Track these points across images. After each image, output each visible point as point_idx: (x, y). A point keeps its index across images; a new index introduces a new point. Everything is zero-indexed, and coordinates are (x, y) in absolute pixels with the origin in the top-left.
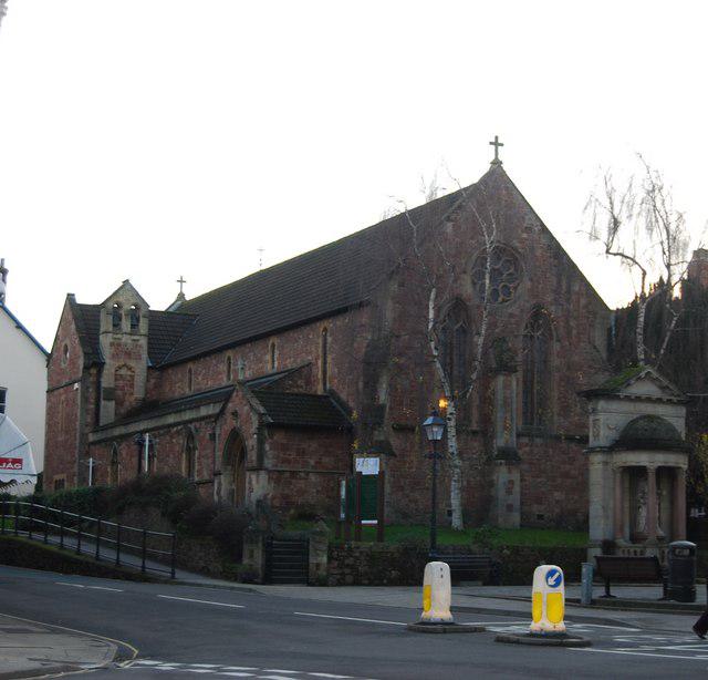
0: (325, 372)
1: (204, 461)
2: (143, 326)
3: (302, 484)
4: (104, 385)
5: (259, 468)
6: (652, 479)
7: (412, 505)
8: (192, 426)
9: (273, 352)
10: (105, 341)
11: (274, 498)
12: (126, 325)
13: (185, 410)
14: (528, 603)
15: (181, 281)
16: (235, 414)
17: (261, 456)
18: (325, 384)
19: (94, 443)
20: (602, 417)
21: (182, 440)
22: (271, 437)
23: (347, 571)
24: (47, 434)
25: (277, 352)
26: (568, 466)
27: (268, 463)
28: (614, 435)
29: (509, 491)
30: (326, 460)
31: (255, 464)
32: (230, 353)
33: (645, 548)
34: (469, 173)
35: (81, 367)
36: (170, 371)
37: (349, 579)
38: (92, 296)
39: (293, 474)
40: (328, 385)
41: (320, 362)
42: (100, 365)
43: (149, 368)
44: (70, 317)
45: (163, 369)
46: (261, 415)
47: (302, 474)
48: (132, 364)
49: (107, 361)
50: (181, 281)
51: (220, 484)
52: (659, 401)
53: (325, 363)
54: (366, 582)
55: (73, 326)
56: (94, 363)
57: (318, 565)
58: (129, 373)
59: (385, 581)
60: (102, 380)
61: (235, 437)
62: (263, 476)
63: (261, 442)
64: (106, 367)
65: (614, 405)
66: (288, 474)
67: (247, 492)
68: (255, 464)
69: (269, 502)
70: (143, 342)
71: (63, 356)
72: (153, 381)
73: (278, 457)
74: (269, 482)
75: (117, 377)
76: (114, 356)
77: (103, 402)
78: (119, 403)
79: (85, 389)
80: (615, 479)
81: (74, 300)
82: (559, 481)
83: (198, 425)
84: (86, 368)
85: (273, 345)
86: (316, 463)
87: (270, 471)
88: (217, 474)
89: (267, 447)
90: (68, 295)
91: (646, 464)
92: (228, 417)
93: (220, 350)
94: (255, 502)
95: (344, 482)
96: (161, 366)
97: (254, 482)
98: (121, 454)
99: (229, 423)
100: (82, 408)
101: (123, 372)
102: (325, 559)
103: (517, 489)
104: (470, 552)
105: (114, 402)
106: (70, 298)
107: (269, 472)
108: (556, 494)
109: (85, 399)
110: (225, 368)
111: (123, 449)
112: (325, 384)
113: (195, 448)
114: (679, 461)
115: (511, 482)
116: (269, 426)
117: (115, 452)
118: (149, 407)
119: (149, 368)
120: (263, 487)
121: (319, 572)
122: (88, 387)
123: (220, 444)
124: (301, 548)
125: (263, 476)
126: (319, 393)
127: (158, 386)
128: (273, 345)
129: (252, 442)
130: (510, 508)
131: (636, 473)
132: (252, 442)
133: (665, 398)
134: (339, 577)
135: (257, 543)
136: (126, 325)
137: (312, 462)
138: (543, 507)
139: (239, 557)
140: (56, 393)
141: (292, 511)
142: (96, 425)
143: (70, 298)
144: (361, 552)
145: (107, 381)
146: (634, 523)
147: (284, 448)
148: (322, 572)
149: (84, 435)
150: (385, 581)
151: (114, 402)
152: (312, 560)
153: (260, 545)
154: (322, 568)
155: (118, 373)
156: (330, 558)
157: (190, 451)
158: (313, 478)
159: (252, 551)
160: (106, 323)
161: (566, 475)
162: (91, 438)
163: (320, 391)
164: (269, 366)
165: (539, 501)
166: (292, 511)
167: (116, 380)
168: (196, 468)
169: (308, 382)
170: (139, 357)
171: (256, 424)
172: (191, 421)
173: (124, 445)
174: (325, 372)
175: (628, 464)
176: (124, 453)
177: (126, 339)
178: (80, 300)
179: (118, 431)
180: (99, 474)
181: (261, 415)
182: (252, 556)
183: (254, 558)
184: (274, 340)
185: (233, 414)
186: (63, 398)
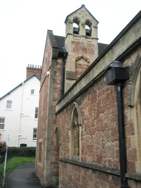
4: (67, 69)
14: (54, 46)
34: (140, 22)
48: (88, 56)
49: (70, 53)
60: (66, 66)
64: (68, 57)
84: (54, 58)
98: (83, 113)
106: (50, 33)
122: (55, 72)
143: (50, 33)
145: (70, 66)
167: (76, 67)
170: (93, 53)
176: (86, 113)
178: (55, 33)
180: (62, 138)
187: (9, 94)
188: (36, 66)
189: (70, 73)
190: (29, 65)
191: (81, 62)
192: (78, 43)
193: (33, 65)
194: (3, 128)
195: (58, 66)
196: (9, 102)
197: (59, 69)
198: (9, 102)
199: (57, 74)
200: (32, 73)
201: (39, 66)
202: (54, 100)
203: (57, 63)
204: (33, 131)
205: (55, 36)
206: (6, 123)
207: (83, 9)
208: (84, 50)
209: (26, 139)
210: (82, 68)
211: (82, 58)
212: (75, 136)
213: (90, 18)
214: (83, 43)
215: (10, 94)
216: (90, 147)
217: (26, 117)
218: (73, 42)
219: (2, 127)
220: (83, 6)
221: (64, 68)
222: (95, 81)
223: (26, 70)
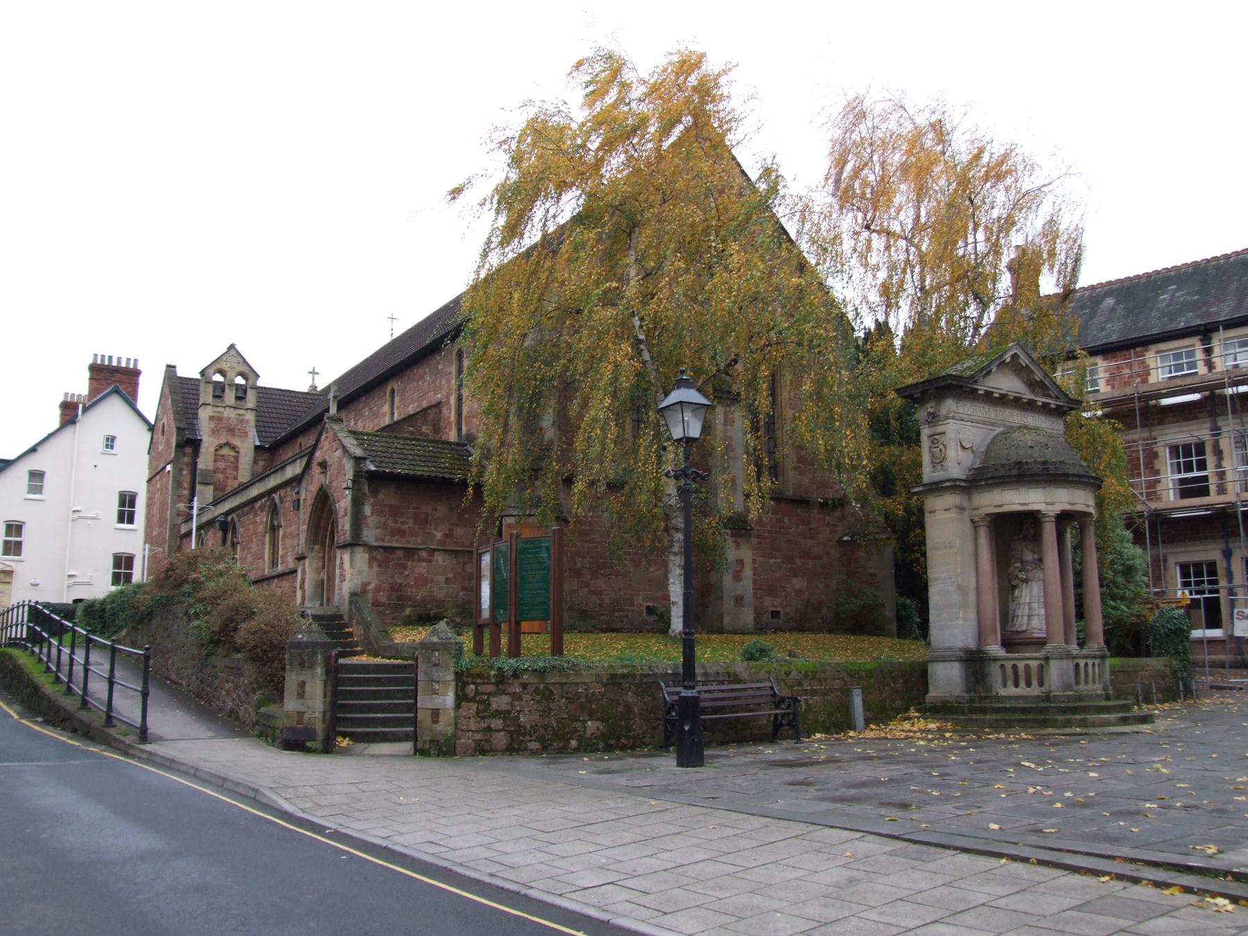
0: (459, 414)
1: (289, 542)
3: (422, 568)
5: (353, 544)
6: (1049, 531)
7: (594, 600)
8: (276, 496)
9: (393, 401)
10: (204, 414)
11: (378, 589)
12: (230, 397)
13: (268, 475)
15: (314, 373)
16: (323, 465)
17: (358, 522)
18: (459, 430)
20: (951, 428)
21: (263, 517)
22: (374, 492)
23: (497, 723)
25: (397, 399)
26: (809, 542)
28: (967, 459)
29: (737, 577)
33: (1047, 659)
37: (500, 739)
38: (189, 370)
39: (410, 552)
40: (464, 429)
41: (453, 400)
42: (195, 444)
43: (257, 448)
44: (167, 391)
46: (358, 460)
47: (424, 554)
48: (236, 442)
50: (314, 373)
51: (304, 572)
52: (1030, 406)
53: (460, 399)
54: (534, 745)
56: (189, 444)
57: (435, 713)
58: (233, 453)
59: (574, 743)
60: (199, 460)
61: (324, 500)
62: (362, 556)
63: (357, 503)
64: (204, 445)
65: (967, 409)
66: (400, 553)
67: (337, 581)
69: (370, 596)
70: (250, 417)
73: (385, 527)
74: (370, 566)
76: (214, 432)
77: (198, 487)
79: (178, 471)
80: (976, 539)
81: (175, 372)
82: (798, 561)
83: (282, 492)
84: (180, 446)
85: (393, 391)
86: (445, 535)
88: (301, 558)
89: (367, 510)
91: (1042, 507)
92: (316, 470)
94: (347, 597)
95: (486, 559)
97: (347, 565)
99: (316, 479)
100: (173, 495)
102: (449, 699)
103: (748, 572)
104: (735, 678)
105: (211, 488)
106: (171, 369)
108: (795, 580)
112: (459, 430)
114: (1080, 500)
115: (740, 562)
116: (373, 477)
119: (257, 448)
120: (360, 573)
122: (181, 469)
123: (305, 514)
124: (404, 679)
126: (452, 440)
128: (393, 391)
129: (344, 503)
130: (739, 600)
131: (1027, 523)
132: (344, 503)
133: (1040, 400)
134: (478, 736)
135: (312, 667)
136: (230, 397)
137: (439, 535)
138: (779, 600)
139: (277, 692)
141: (408, 611)
143: (171, 369)
144: (524, 686)
145: (205, 461)
146: (1006, 615)
147: (395, 512)
148: (444, 727)
150: (574, 743)
151: (211, 488)
152: (425, 702)
153: (319, 671)
154: (443, 718)
155: (221, 452)
156: (461, 698)
157: (274, 529)
158: (439, 558)
159: (302, 685)
160: (206, 395)
161: (807, 554)
163: (452, 436)
165: (772, 592)
166: (408, 611)
167: (215, 461)
168: (280, 553)
169: (437, 429)
170: (245, 434)
171: (350, 474)
174: (459, 414)
175: (1006, 509)
177: (229, 414)
178: (181, 373)
181: (358, 460)
182: (301, 695)
183: (307, 697)
184: (395, 384)
185: (320, 464)
187: (33, 450)
188: (119, 359)
189: (205, 473)
190: (96, 355)
191: (225, 451)
192: (220, 419)
193: (110, 358)
195: (186, 459)
197: (187, 464)
198: (37, 476)
199: (184, 473)
200: (109, 384)
201: (128, 359)
202: (178, 515)
203: (184, 455)
204: (110, 562)
205: (180, 378)
207: (233, 352)
208: (231, 430)
209: (89, 584)
210: (226, 461)
211: (227, 444)
214: (229, 418)
215: (39, 449)
217: (89, 522)
218: (212, 418)
220: (232, 347)
221: (195, 464)
223: (87, 374)
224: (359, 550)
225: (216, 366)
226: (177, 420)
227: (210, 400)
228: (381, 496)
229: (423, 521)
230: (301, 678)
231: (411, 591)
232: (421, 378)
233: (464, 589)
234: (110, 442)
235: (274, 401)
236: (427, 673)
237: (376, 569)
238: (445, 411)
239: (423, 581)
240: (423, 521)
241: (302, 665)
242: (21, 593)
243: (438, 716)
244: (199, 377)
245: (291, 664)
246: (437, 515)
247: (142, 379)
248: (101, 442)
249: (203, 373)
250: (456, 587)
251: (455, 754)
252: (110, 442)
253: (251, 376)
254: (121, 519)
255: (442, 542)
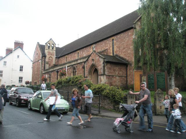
2: (55, 49)
3: (115, 79)
4: (46, 61)
8: (75, 66)
10: (46, 51)
12: (51, 48)
17: (104, 71)
19: (44, 73)
24: (33, 72)
27: (106, 73)
30: (120, 72)
31: (102, 73)
32: (79, 51)
35: (41, 57)
36: (61, 58)
38: (43, 43)
41: (111, 48)
45: (59, 58)
47: (115, 77)
48: (52, 57)
53: (113, 48)
55: (39, 49)
56: (44, 56)
62: (105, 77)
64: (47, 57)
68: (102, 73)
70: (55, 52)
71: (36, 55)
72: (57, 60)
75: (49, 59)
77: (46, 65)
78: (50, 65)
79: (42, 62)
83: (77, 65)
84: (42, 57)
86: (118, 73)
87: (107, 75)
89: (106, 68)
90: (20, 66)
93: (65, 55)
96: (58, 58)
98: (52, 75)
101: (50, 58)
106: (38, 43)
107: (107, 76)
109: (42, 64)
110: (77, 55)
111: (52, 74)
113: (76, 72)
117: (50, 75)
118: (55, 66)
121: (162, 110)
125: (105, 77)
127: (58, 62)
136: (51, 48)
137: (117, 73)
140: (35, 63)
142: (44, 70)
143: (38, 43)
145: (47, 60)
147: (110, 69)
149: (42, 72)
158: (117, 77)
160: (46, 48)
162: (43, 72)
164: (77, 57)
172: (74, 65)
173: (52, 73)
178: (40, 44)
179: (51, 70)
186: (36, 64)
188: (20, 41)
189: (47, 62)
191: (50, 58)
194: (2, 76)
196: (5, 62)
198: (5, 62)
206: (4, 74)
208: (51, 54)
210: (50, 60)
212: (142, 50)
213: (53, 43)
216: (53, 81)
218: (48, 52)
219: (2, 76)
221: (45, 60)
222: (54, 70)
224: (105, 76)
225: (48, 42)
226: (42, 52)
227: (48, 49)
228: (108, 66)
229: (114, 70)
230: (131, 100)
231: (113, 84)
232: (101, 44)
233: (121, 83)
234: (18, 56)
235: (58, 49)
236: (159, 99)
237: (107, 79)
238: (109, 51)
239: (115, 82)
240: (114, 70)
241: (131, 98)
242: (2, 83)
243: (161, 107)
244: (45, 45)
245: (129, 97)
246: (117, 69)
247: (24, 45)
248: (17, 56)
249: (46, 44)
250: (120, 83)
251: (73, 110)
252: (18, 56)
253: (54, 45)
254: (20, 71)
255: (118, 75)
